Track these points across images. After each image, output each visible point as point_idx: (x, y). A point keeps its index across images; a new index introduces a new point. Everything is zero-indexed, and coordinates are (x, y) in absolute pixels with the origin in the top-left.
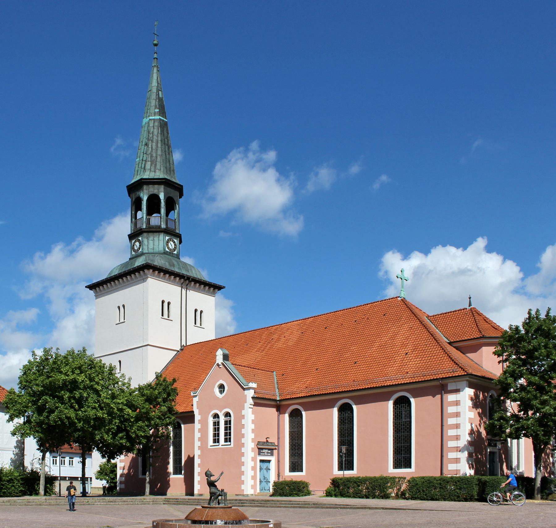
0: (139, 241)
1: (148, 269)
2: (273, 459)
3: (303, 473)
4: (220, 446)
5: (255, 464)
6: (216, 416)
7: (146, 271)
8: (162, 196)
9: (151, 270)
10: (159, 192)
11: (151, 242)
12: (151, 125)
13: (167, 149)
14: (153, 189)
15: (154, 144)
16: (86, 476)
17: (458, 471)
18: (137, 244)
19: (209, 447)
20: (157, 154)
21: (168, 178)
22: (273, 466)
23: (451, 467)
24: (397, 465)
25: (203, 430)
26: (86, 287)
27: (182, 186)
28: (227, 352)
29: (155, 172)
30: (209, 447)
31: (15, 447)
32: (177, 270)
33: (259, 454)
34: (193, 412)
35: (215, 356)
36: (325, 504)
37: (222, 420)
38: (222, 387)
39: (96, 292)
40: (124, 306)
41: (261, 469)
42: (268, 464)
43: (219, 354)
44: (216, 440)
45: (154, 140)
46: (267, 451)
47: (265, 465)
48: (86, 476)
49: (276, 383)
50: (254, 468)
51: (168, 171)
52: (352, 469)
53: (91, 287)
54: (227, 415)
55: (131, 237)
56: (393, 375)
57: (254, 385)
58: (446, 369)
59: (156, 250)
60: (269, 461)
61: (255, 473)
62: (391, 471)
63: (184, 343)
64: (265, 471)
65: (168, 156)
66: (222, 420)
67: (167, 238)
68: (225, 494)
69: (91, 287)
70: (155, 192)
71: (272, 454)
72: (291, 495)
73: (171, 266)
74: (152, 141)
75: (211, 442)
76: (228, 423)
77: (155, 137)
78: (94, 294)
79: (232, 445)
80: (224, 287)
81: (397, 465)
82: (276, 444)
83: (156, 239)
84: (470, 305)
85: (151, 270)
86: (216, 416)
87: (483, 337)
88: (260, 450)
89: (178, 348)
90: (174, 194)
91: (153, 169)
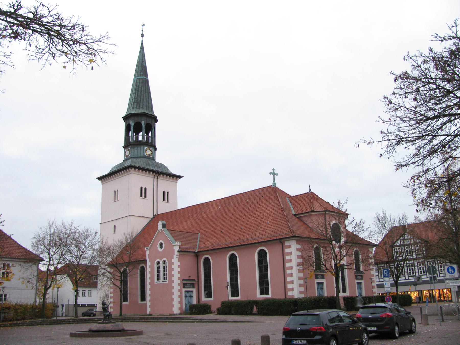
0: (129, 150)
1: (131, 168)
2: (194, 290)
3: (212, 299)
4: (161, 283)
5: (181, 293)
6: (159, 263)
7: (130, 169)
8: (143, 123)
9: (133, 169)
10: (141, 121)
11: (136, 151)
12: (138, 81)
13: (147, 96)
14: (137, 120)
15: (139, 93)
16: (78, 303)
17: (293, 296)
18: (128, 152)
19: (155, 283)
20: (140, 99)
21: (146, 112)
22: (195, 294)
23: (290, 293)
24: (262, 293)
25: (152, 272)
26: (96, 179)
27: (156, 116)
28: (164, 222)
29: (139, 109)
30: (155, 283)
31: (382, 221)
32: (152, 168)
33: (184, 287)
34: (146, 260)
35: (158, 225)
36: (206, 320)
37: (162, 266)
38: (161, 244)
39: (102, 182)
40: (118, 190)
41: (186, 297)
42: (191, 293)
43: (160, 223)
44: (159, 279)
45: (140, 91)
46: (189, 285)
47: (188, 295)
48: (78, 303)
49: (198, 241)
50: (180, 297)
51: (148, 108)
52: (238, 296)
53: (100, 179)
54: (165, 262)
55: (124, 147)
56: (258, 236)
57: (179, 243)
58: (284, 232)
59: (139, 155)
60: (192, 291)
61: (182, 299)
62: (231, 298)
63: (155, 213)
64: (189, 298)
65: (147, 99)
66: (162, 266)
67: (146, 148)
68: (111, 315)
69: (100, 179)
70: (139, 121)
71: (194, 287)
72: (199, 314)
73: (147, 165)
74: (138, 91)
75: (156, 279)
76: (165, 267)
77: (140, 89)
78: (101, 183)
79: (167, 282)
80: (183, 177)
81: (262, 293)
82: (196, 280)
83: (139, 149)
84: (310, 190)
85: (133, 169)
86: (159, 263)
87: (313, 211)
88: (185, 285)
89: (152, 216)
90: (151, 121)
91: (138, 107)
